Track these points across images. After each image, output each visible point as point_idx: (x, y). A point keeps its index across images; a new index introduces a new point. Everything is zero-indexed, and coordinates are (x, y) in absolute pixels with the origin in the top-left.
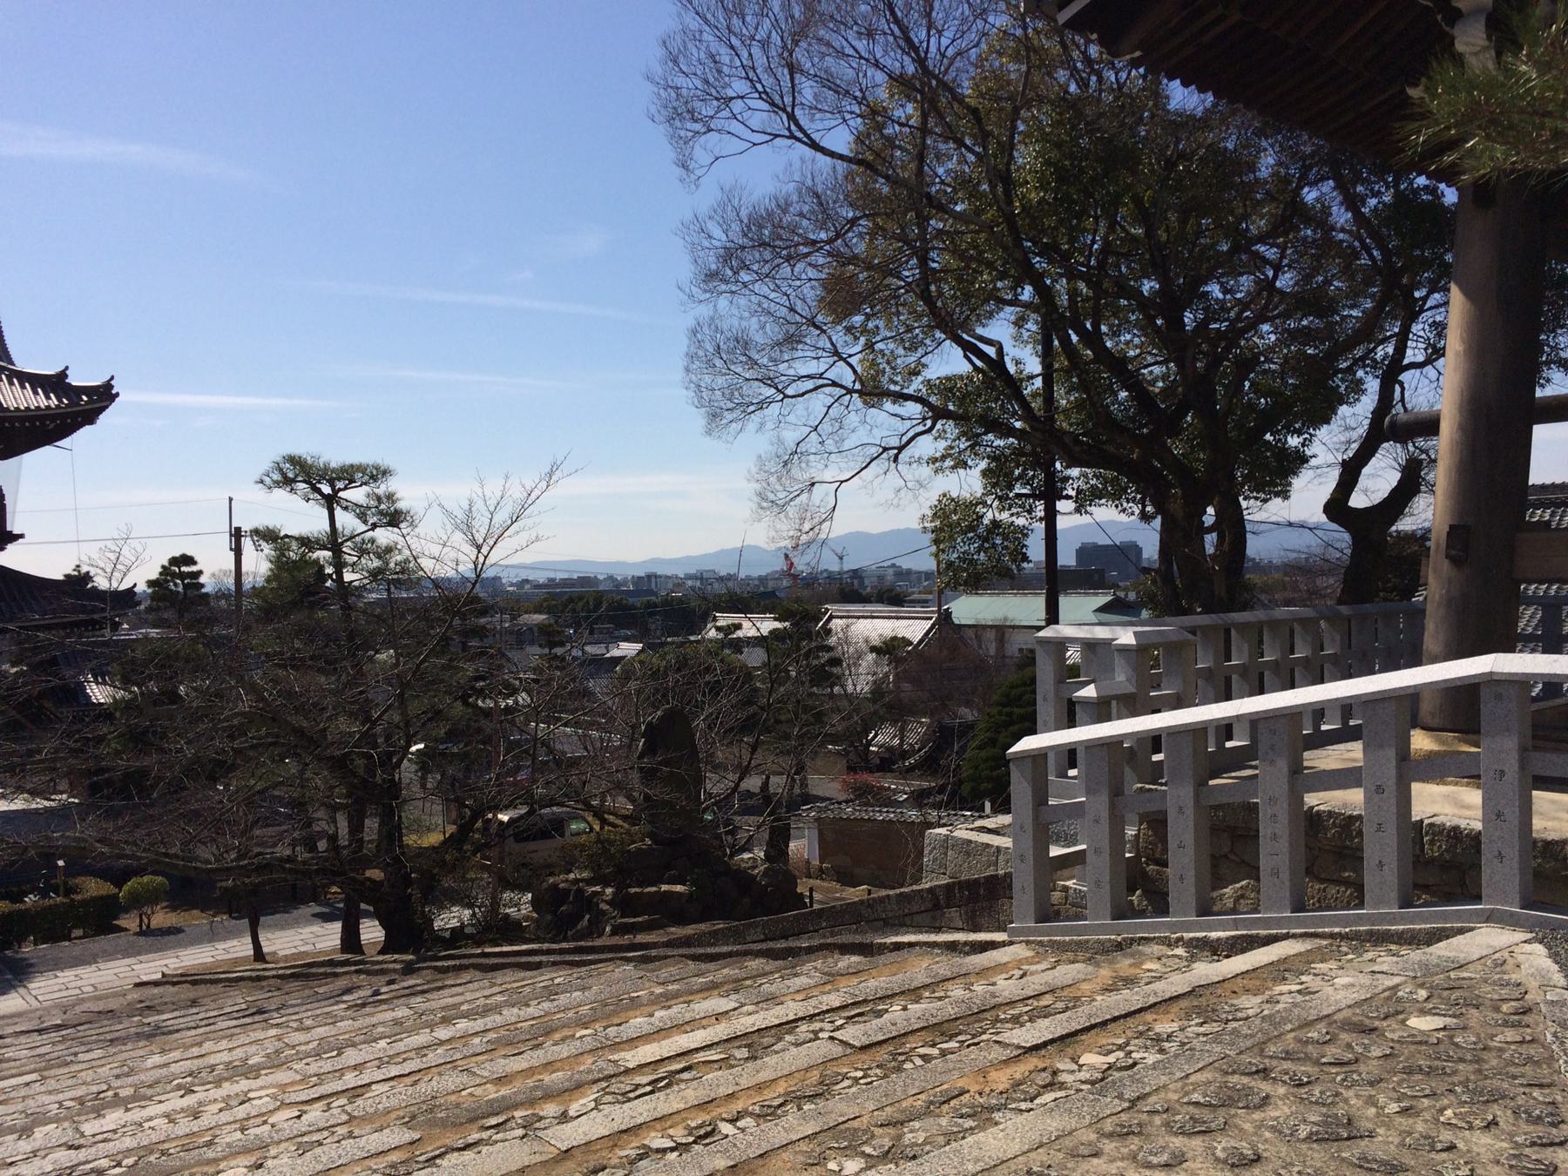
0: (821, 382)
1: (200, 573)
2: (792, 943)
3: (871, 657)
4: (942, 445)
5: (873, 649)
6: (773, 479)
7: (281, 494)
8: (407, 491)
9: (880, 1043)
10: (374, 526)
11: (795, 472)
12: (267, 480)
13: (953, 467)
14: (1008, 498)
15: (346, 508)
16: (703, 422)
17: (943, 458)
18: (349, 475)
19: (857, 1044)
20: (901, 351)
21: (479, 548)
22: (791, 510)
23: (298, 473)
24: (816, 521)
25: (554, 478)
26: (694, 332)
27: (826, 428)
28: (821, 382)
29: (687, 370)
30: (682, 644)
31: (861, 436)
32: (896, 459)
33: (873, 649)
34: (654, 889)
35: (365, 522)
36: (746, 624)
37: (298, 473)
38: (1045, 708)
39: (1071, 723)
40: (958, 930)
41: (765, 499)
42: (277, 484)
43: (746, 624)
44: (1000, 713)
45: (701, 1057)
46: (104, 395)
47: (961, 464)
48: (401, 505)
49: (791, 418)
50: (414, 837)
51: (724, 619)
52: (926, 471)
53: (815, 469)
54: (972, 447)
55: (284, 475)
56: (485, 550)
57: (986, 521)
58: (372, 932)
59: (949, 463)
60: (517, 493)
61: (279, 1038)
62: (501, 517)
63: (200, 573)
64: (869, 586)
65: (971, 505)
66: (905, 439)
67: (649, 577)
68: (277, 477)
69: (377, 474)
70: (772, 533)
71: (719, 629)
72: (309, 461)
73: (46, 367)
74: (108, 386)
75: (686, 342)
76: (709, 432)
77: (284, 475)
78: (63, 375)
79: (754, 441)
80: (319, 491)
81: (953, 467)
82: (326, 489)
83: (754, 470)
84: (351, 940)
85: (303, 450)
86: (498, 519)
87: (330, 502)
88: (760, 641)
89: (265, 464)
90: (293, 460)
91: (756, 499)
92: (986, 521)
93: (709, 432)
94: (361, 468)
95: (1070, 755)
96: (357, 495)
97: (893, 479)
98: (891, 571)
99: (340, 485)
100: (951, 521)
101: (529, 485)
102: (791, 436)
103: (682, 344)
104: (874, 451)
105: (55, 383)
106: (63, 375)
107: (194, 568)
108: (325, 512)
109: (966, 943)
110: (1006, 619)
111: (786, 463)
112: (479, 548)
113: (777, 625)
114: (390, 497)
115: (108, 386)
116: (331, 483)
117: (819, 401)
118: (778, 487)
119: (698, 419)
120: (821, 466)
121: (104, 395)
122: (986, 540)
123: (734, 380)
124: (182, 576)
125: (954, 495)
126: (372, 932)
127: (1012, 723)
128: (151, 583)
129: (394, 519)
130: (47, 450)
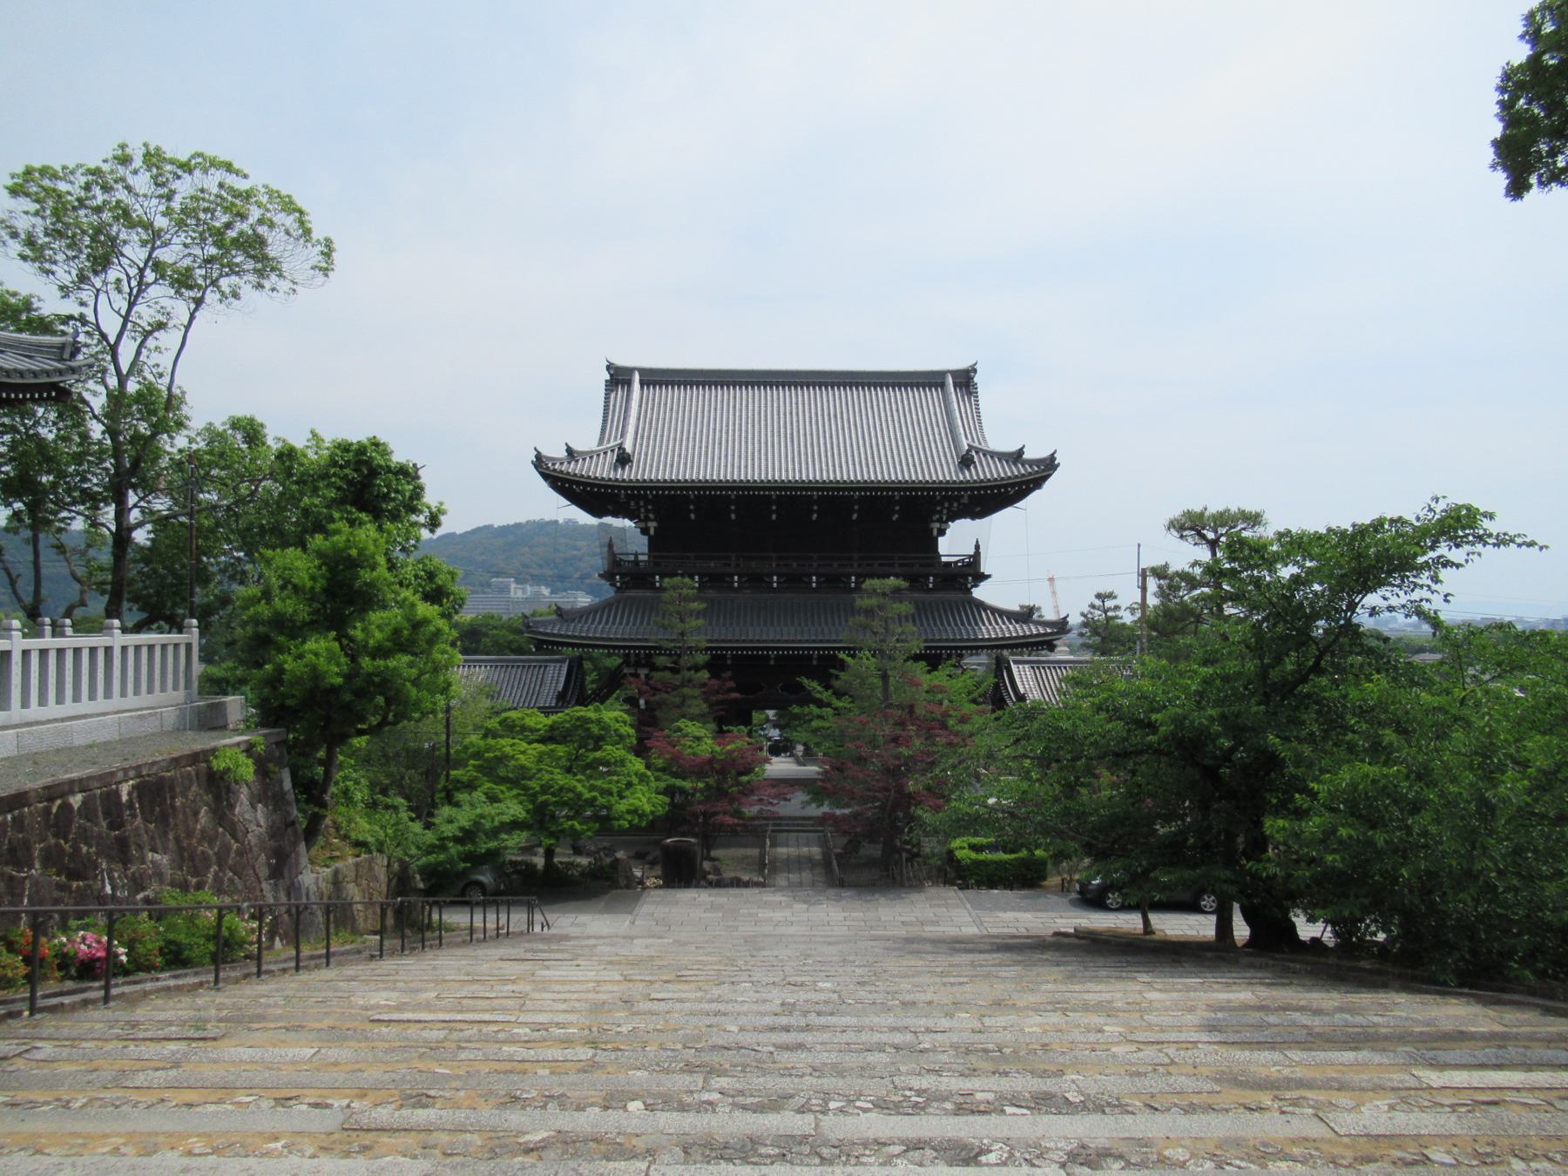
46: (1048, 466)
74: (1052, 457)
78: (1021, 452)
80: (1203, 537)
106: (1021, 452)
115: (1052, 457)
121: (1048, 466)
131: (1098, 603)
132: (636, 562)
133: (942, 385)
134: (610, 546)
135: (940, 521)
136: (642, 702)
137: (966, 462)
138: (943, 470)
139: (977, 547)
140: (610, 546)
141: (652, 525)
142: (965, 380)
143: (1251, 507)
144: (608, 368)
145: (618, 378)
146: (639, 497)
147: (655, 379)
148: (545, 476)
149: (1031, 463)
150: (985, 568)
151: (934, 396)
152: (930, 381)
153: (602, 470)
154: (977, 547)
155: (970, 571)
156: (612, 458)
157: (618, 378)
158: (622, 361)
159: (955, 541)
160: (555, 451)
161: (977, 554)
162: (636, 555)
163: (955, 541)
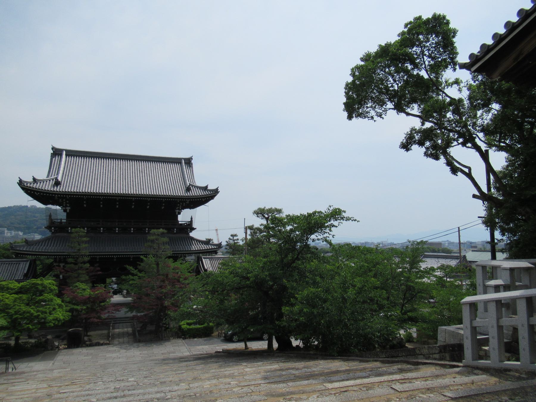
2: (394, 359)
9: (407, 391)
19: (399, 390)
38: (480, 288)
39: (485, 292)
40: (447, 361)
45: (350, 388)
46: (216, 192)
58: (275, 345)
61: (243, 369)
64: (479, 247)
67: (366, 243)
73: (203, 185)
78: (207, 187)
80: (264, 216)
82: (266, 216)
84: (270, 345)
89: (256, 208)
95: (486, 303)
98: (447, 242)
105: (205, 188)
106: (207, 187)
109: (449, 365)
121: (216, 192)
126: (275, 345)
131: (231, 238)
132: (61, 222)
133: (61, 155)
135: (179, 209)
136: (61, 276)
137: (188, 189)
138: (180, 192)
139: (192, 218)
141: (68, 209)
142: (189, 162)
143: (278, 207)
144: (53, 149)
145: (56, 153)
147: (71, 154)
148: (23, 189)
149: (210, 190)
150: (194, 226)
151: (177, 166)
152: (176, 161)
153: (48, 187)
154: (192, 218)
155: (189, 227)
156: (52, 183)
157: (56, 153)
158: (58, 146)
159: (184, 216)
160: (28, 178)
161: (191, 221)
162: (61, 220)
163: (184, 216)
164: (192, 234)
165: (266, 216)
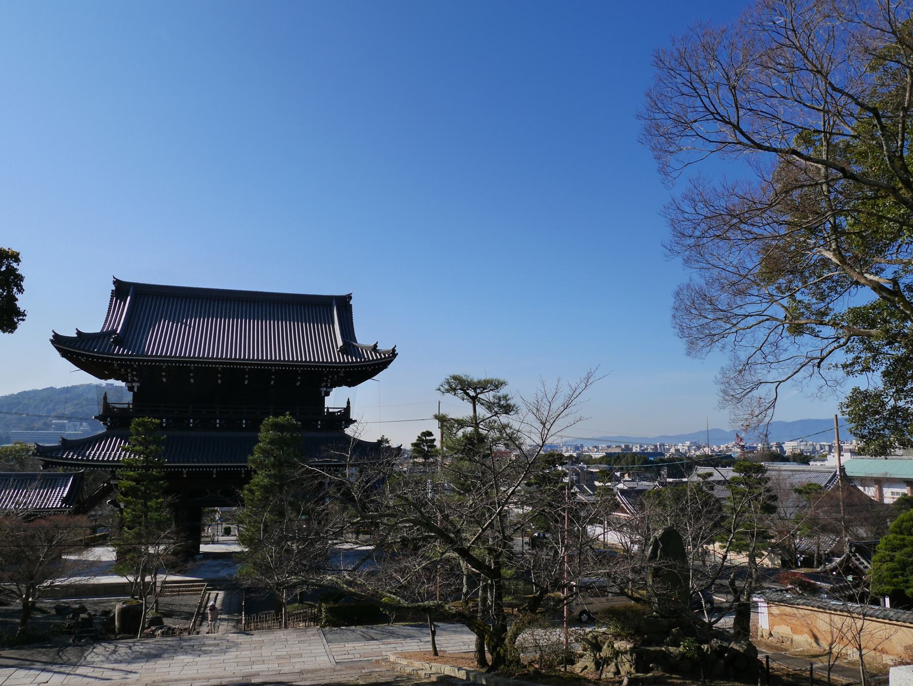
0: (761, 318)
1: (434, 440)
3: (795, 495)
4: (851, 356)
5: (796, 491)
6: (732, 382)
7: (449, 396)
8: (512, 391)
10: (496, 413)
11: (748, 377)
12: (442, 389)
13: (862, 371)
14: (902, 391)
15: (482, 404)
16: (685, 347)
17: (852, 364)
18: (483, 386)
20: (814, 301)
21: (544, 424)
22: (746, 401)
23: (460, 386)
24: (763, 408)
25: (590, 381)
26: (678, 294)
27: (766, 349)
28: (761, 318)
29: (674, 317)
30: (677, 484)
31: (792, 351)
32: (819, 366)
33: (796, 491)
34: (658, 648)
35: (491, 411)
36: (716, 474)
37: (460, 386)
41: (728, 395)
42: (448, 391)
43: (716, 474)
44: (895, 538)
47: (866, 369)
48: (511, 402)
49: (743, 343)
50: (599, 530)
51: (702, 470)
52: (841, 373)
53: (761, 373)
54: (874, 357)
55: (451, 386)
56: (548, 425)
57: (888, 407)
59: (857, 368)
60: (566, 391)
62: (557, 405)
63: (434, 440)
65: (878, 396)
66: (825, 353)
68: (447, 387)
69: (497, 385)
70: (733, 417)
71: (699, 476)
72: (464, 378)
74: (394, 350)
75: (673, 300)
76: (689, 354)
77: (451, 386)
78: (375, 346)
79: (718, 359)
80: (468, 394)
81: (862, 371)
82: (472, 393)
83: (719, 376)
85: (461, 372)
86: (555, 406)
87: (474, 400)
88: (724, 482)
89: (442, 380)
90: (455, 378)
91: (721, 394)
92: (888, 407)
93: (689, 354)
94: (487, 382)
96: (488, 396)
97: (817, 381)
99: (478, 391)
100: (863, 407)
101: (574, 385)
102: (743, 356)
103: (671, 301)
104: (803, 360)
106: (375, 346)
107: (432, 438)
108: (471, 405)
110: (886, 474)
111: (740, 372)
112: (544, 424)
113: (737, 475)
114: (505, 397)
115: (394, 350)
116: (475, 389)
117: (761, 333)
118: (737, 387)
119: (681, 345)
120: (765, 372)
121: (393, 354)
122: (888, 420)
123: (702, 319)
124: (427, 441)
125: (862, 389)
127: (905, 546)
128: (413, 445)
129: (508, 409)
130: (368, 382)
134: (105, 398)
135: (326, 386)
139: (348, 403)
140: (105, 398)
141: (136, 385)
142: (344, 304)
146: (128, 366)
150: (353, 416)
154: (348, 403)
155: (345, 418)
159: (335, 399)
163: (335, 399)
164: (349, 431)
165: (472, 393)
